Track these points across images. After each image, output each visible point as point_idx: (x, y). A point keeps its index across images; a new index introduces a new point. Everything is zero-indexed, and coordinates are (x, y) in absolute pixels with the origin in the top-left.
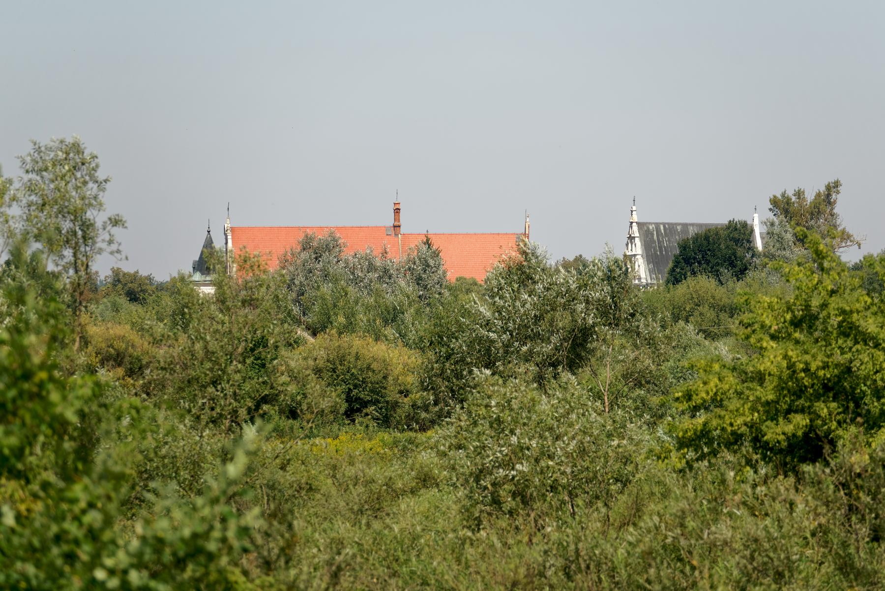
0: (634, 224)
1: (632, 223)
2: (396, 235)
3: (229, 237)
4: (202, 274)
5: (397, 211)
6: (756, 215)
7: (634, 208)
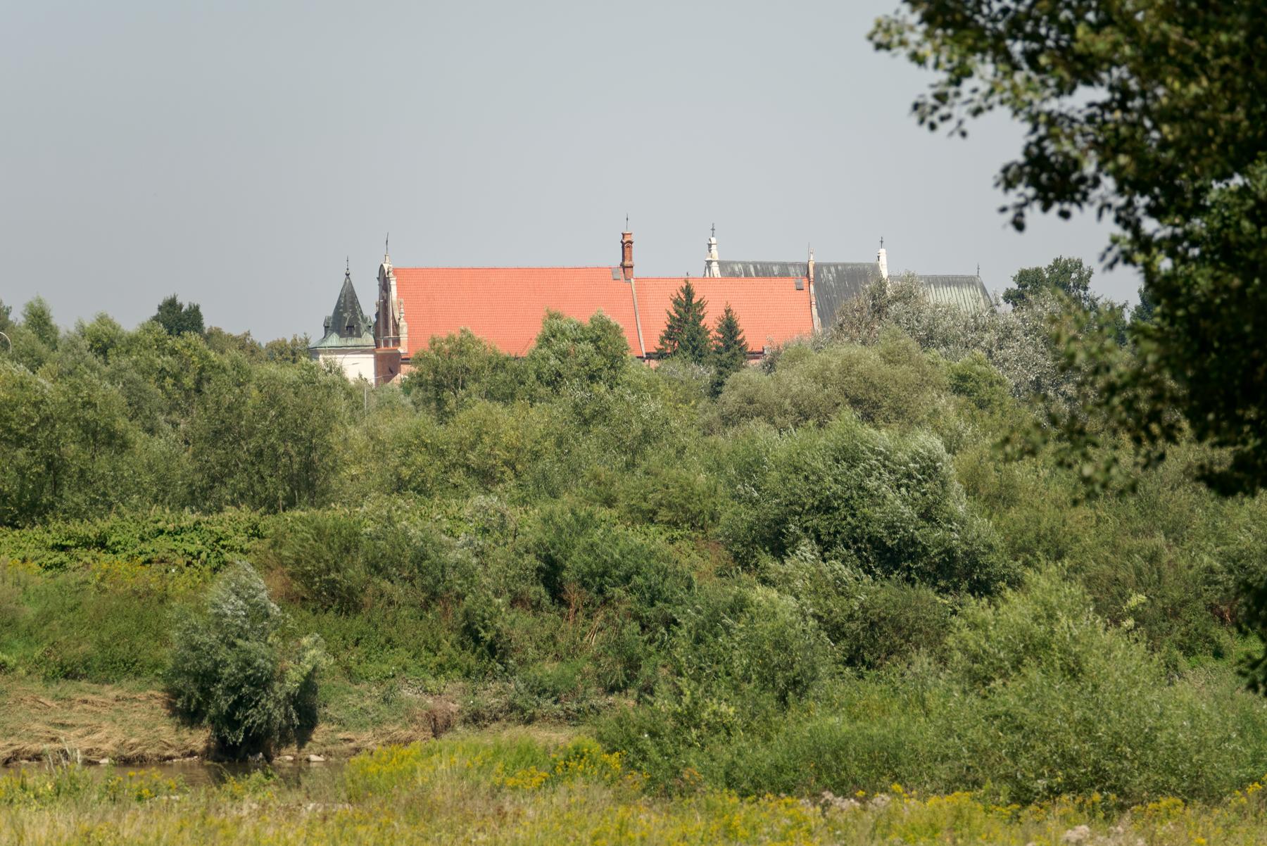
0: (714, 265)
1: (709, 262)
2: (628, 279)
3: (393, 283)
4: (342, 336)
5: (626, 246)
6: (883, 251)
7: (714, 240)
